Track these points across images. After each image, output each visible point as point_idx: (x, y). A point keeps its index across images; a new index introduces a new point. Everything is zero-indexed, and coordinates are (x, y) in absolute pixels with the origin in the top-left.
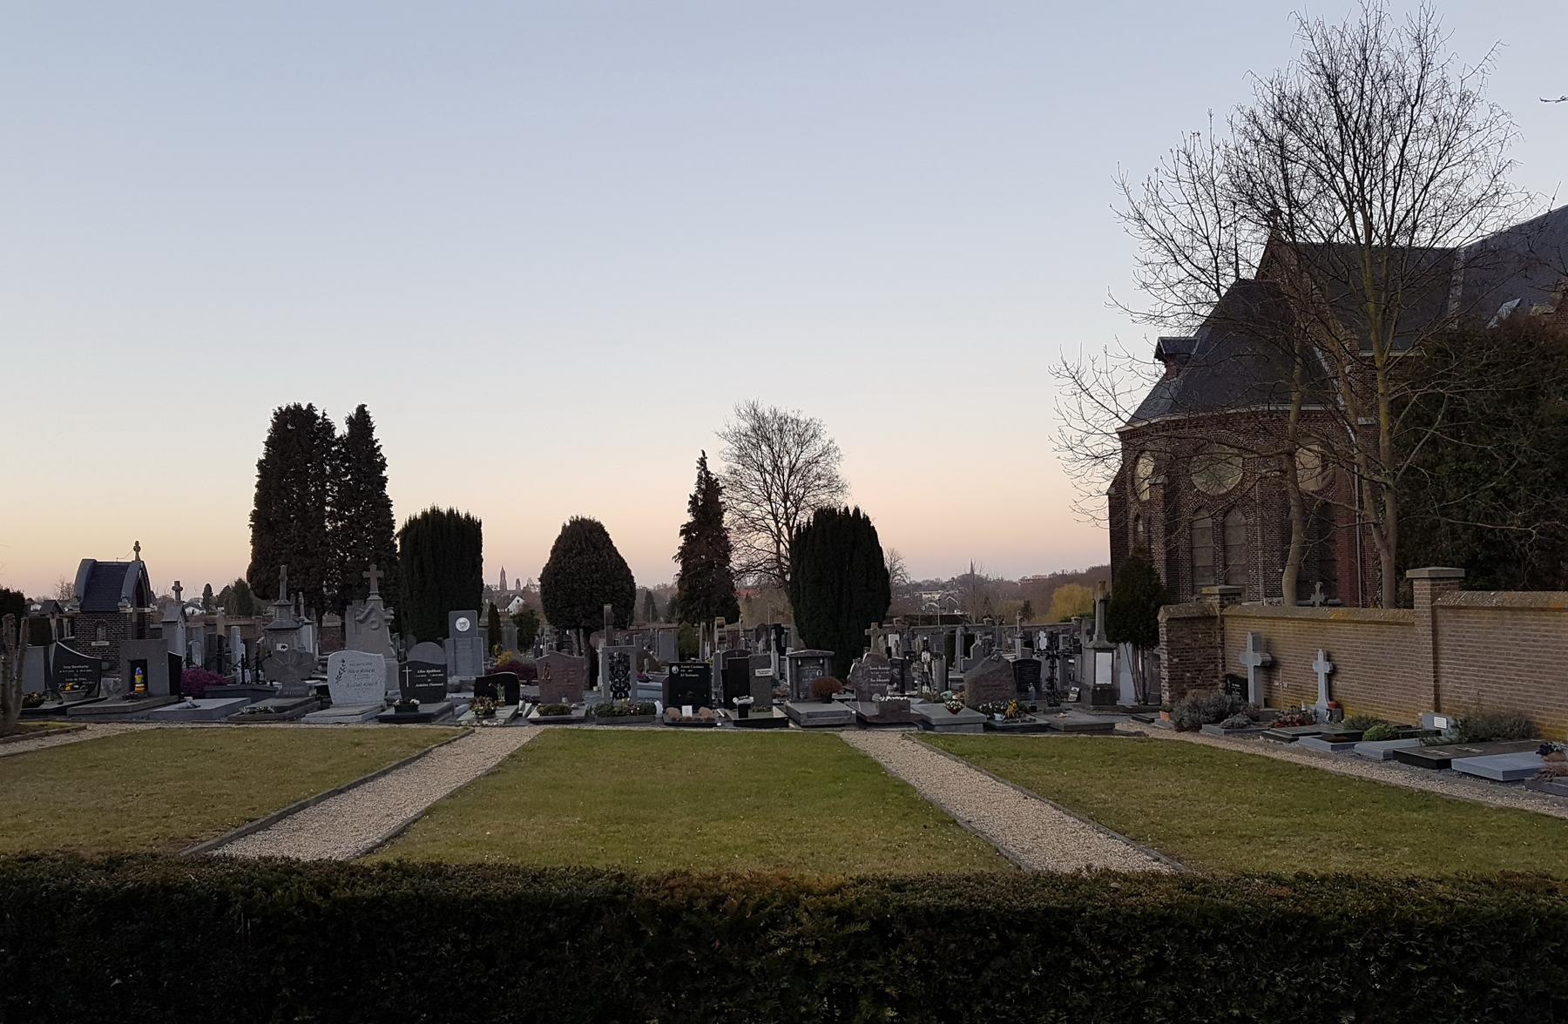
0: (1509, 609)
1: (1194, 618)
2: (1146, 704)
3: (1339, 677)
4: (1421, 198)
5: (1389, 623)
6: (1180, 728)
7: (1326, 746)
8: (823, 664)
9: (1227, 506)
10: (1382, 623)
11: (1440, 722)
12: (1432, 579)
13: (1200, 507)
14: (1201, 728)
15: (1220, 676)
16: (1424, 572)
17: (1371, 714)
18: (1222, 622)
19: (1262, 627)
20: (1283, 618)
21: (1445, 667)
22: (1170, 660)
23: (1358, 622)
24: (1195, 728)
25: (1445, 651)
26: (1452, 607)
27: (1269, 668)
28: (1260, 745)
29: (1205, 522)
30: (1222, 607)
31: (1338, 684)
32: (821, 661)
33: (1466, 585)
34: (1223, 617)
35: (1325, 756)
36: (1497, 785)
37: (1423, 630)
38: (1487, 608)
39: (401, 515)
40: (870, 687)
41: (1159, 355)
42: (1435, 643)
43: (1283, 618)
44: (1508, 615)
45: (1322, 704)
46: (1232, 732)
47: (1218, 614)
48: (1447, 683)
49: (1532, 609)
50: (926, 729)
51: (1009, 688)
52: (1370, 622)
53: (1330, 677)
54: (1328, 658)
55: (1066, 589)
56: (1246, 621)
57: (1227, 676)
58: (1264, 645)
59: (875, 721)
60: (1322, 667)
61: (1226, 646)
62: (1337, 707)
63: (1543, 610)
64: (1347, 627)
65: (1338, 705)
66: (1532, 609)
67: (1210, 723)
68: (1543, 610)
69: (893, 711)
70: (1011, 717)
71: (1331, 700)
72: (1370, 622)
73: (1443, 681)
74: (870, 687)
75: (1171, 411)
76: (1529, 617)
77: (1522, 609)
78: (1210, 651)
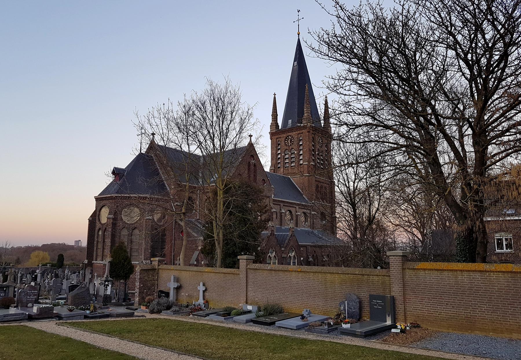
0: (274, 270)
1: (149, 269)
2: (118, 302)
3: (207, 291)
4: (512, 133)
5: (229, 273)
6: (152, 312)
7: (222, 319)
8: (6, 290)
9: (133, 228)
10: (226, 273)
11: (250, 308)
12: (247, 259)
13: (136, 228)
14: (161, 312)
15: (156, 291)
16: (245, 257)
17: (232, 306)
18: (158, 271)
19: (177, 273)
20: (185, 270)
21: (250, 289)
22: (140, 285)
23: (217, 273)
24: (159, 312)
25: (250, 283)
26: (254, 269)
27: (178, 289)
28: (191, 318)
29: (125, 232)
30: (159, 265)
31: (207, 294)
32: (5, 289)
33: (255, 262)
34: (158, 269)
35: (222, 322)
36: (294, 331)
37: (243, 275)
38: (266, 270)
39: (269, 171)
40: (27, 300)
41: (113, 173)
42: (247, 281)
43: (185, 270)
44: (273, 272)
45: (201, 301)
46: (176, 314)
47: (157, 268)
48: (250, 294)
49: (282, 271)
50: (59, 320)
51: (88, 299)
52: (222, 273)
53: (204, 292)
54: (204, 285)
55: (36, 253)
56: (168, 271)
57: (159, 291)
58: (177, 280)
59: (37, 317)
60: (201, 288)
61: (159, 280)
62: (207, 303)
63: (286, 271)
64: (212, 274)
65: (207, 302)
66: (282, 271)
67: (164, 310)
68: (286, 271)
69: (46, 312)
70: (92, 312)
71: (204, 300)
72: (222, 273)
73: (249, 293)
74: (27, 300)
75: (117, 193)
76: (281, 273)
77: (279, 270)
78: (153, 282)
